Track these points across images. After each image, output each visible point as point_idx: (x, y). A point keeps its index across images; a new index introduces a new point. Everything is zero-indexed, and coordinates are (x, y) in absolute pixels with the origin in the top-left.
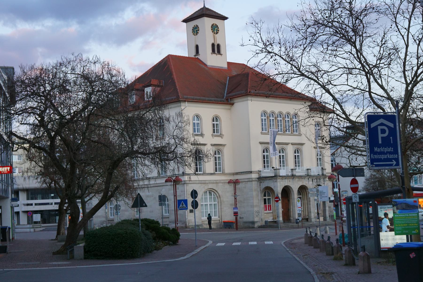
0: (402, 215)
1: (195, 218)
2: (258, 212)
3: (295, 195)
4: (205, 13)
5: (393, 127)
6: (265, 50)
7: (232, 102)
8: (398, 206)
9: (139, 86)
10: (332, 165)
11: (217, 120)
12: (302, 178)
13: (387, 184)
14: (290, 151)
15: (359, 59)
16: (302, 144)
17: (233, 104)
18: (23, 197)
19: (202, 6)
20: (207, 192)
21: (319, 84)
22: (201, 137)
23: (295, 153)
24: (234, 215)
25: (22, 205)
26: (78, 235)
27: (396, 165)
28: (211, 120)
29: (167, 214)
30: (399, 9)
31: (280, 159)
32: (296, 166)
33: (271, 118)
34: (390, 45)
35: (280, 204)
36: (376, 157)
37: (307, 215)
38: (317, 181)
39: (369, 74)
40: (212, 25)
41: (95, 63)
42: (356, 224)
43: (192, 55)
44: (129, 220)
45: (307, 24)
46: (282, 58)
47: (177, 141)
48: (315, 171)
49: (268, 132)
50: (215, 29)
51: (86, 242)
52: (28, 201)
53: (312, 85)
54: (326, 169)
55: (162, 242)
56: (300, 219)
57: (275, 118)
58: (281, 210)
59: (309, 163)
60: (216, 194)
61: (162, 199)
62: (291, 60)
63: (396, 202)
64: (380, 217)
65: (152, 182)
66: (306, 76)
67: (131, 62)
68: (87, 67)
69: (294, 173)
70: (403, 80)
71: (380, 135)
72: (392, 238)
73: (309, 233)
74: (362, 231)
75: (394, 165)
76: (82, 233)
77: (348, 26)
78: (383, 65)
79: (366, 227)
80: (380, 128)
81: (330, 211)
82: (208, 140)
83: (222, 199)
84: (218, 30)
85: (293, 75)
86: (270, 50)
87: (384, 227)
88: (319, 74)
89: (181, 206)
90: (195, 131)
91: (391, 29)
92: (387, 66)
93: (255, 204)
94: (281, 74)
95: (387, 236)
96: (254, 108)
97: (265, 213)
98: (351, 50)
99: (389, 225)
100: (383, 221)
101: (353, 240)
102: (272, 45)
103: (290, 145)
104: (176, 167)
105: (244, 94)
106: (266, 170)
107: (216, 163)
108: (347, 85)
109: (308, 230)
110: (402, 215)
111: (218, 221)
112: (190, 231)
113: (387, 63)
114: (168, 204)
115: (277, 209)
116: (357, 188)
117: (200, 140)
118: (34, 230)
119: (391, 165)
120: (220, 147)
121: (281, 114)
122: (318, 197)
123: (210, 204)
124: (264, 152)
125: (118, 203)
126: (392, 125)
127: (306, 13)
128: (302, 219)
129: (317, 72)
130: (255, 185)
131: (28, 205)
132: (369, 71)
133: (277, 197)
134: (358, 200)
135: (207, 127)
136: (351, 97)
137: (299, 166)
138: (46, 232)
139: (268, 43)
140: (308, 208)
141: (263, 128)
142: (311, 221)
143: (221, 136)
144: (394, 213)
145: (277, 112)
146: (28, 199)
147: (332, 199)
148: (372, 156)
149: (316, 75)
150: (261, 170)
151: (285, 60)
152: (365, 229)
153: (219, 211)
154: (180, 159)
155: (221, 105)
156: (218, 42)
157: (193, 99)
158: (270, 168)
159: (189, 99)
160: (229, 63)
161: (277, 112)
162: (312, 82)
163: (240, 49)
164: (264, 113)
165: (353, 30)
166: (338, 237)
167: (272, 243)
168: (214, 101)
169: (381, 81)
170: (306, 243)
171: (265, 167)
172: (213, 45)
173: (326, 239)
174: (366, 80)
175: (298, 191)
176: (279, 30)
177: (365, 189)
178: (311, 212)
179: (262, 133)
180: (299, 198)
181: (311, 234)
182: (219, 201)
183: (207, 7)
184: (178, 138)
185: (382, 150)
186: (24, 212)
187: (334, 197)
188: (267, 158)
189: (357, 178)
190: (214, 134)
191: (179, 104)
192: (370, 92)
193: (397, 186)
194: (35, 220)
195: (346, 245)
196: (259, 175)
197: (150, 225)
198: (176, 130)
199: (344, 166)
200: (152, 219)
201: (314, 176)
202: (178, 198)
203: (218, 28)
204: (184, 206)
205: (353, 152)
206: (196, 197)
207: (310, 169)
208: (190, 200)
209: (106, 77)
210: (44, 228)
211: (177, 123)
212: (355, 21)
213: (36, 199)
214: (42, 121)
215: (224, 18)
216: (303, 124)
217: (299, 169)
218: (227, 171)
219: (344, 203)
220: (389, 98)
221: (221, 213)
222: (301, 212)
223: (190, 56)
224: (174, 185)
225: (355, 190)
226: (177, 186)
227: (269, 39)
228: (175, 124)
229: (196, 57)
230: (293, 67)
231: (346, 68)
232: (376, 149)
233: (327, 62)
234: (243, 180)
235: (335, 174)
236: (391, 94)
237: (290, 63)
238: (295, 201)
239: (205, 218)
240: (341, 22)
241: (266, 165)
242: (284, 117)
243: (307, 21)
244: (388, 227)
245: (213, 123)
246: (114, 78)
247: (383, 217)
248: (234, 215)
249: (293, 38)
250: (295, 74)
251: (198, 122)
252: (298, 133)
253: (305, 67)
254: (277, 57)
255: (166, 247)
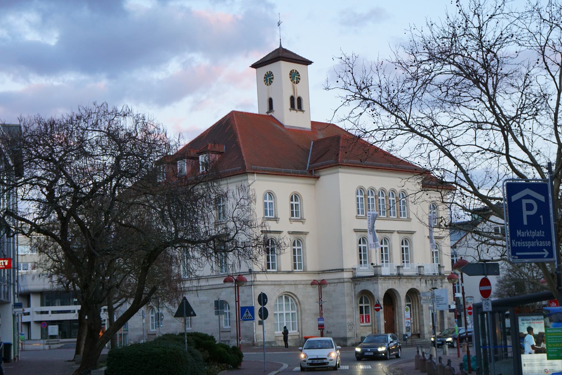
0: (557, 331)
1: (268, 331)
2: (352, 325)
3: (402, 302)
4: (281, 55)
5: (544, 201)
6: (359, 96)
7: (317, 175)
8: (552, 316)
9: (193, 154)
10: (453, 261)
11: (296, 199)
12: (412, 279)
13: (527, 288)
14: (396, 241)
15: (494, 109)
16: (412, 233)
17: (318, 178)
18: (35, 301)
19: (278, 47)
20: (282, 297)
21: (435, 144)
22: (275, 222)
23: (402, 244)
24: (319, 329)
25: (34, 313)
26: (99, 355)
27: (548, 257)
28: (288, 199)
29: (228, 327)
30: (547, 40)
31: (382, 252)
32: (404, 262)
33: (370, 197)
34: (535, 89)
35: (381, 314)
36: (520, 244)
37: (418, 329)
38: (432, 283)
39: (505, 129)
40: (291, 72)
41: (125, 115)
42: (487, 343)
43: (264, 111)
44: (172, 334)
45: (418, 59)
46: (384, 107)
47: (238, 225)
48: (430, 269)
49: (366, 215)
50: (295, 77)
51: (107, 365)
52: (42, 307)
53: (426, 145)
54: (444, 267)
55: (218, 366)
56: (409, 334)
57: (375, 196)
58: (382, 323)
59: (422, 257)
60: (295, 300)
61: (220, 306)
62: (396, 110)
63: (548, 311)
64: (522, 333)
65: (203, 283)
66: (416, 132)
67: (181, 123)
68: (114, 122)
69: (401, 271)
70: (554, 139)
71: (525, 213)
72: (539, 362)
73: (421, 354)
74: (496, 352)
75: (545, 256)
76: (105, 351)
77: (477, 61)
78: (526, 116)
79: (501, 346)
80: (524, 202)
81: (450, 324)
82: (284, 225)
83: (302, 307)
84: (300, 79)
85: (399, 131)
86: (367, 96)
87: (527, 347)
88: (435, 130)
89: (245, 315)
90: (266, 214)
91: (537, 65)
92: (531, 117)
93: (347, 314)
94: (381, 130)
95: (532, 360)
96: (347, 183)
97: (361, 326)
98: (481, 95)
99: (535, 344)
100: (527, 338)
101: (483, 365)
102: (368, 89)
103: (396, 233)
104: (237, 261)
105: (332, 165)
106: (363, 268)
107: (295, 257)
108: (476, 145)
109: (420, 350)
110: (557, 331)
111: (297, 337)
112: (257, 350)
113: (532, 113)
114: (229, 313)
115: (378, 321)
116: (490, 291)
117: (272, 226)
118: (50, 347)
119: (542, 256)
120: (301, 236)
121: (383, 191)
122: (433, 304)
123: (286, 314)
124: (360, 243)
125: (160, 311)
126: (542, 198)
127: (417, 45)
128: (412, 335)
129: (433, 127)
130: (347, 287)
131: (42, 313)
132: (505, 125)
133: (378, 305)
134: (490, 309)
135: (283, 208)
136: (480, 162)
137: (407, 262)
138: (63, 350)
139: (363, 86)
140: (419, 319)
141: (358, 210)
142: (424, 338)
143: (302, 220)
144: (546, 327)
145: (377, 188)
146: (42, 305)
147: (453, 307)
148: (513, 243)
149: (431, 130)
150: (356, 267)
151: (387, 110)
152: (499, 349)
153: (298, 323)
154: (244, 251)
155: (302, 178)
156: (299, 94)
157: (264, 171)
158: (368, 264)
159: (259, 170)
160: (313, 123)
161: (377, 188)
162: (426, 140)
163: (327, 105)
164: (361, 190)
165: (483, 66)
166: (461, 360)
167: (370, 368)
168: (293, 173)
169: (523, 140)
170: (417, 369)
171: (361, 263)
172: (292, 98)
173: (445, 363)
174: (503, 138)
175: (406, 296)
176: (379, 67)
177: (499, 294)
178: (423, 325)
179: (357, 217)
180: (407, 305)
181: (423, 355)
182: (299, 310)
183: (284, 47)
184: (239, 220)
185: (528, 234)
186: (37, 322)
187: (456, 304)
188: (364, 251)
189: (489, 277)
190: (292, 218)
191: (245, 178)
192: (508, 156)
193: (546, 289)
194: (50, 333)
195: (472, 372)
196: (354, 274)
197: (202, 341)
198: (237, 210)
199: (470, 260)
200: (204, 332)
201: (428, 276)
202: (241, 305)
203: (299, 76)
204: (250, 315)
205: (483, 240)
206: (265, 303)
207: (423, 267)
208: (258, 307)
209: (139, 136)
210: (63, 345)
211: (239, 200)
212: (486, 55)
213: (53, 305)
214: (51, 196)
215: (307, 63)
216: (412, 200)
217: (407, 266)
218: (309, 269)
219: (470, 313)
220: (534, 164)
221: (302, 325)
222: (410, 325)
223: (261, 113)
224: (235, 287)
225: (486, 294)
226: (241, 289)
227: (365, 81)
228: (235, 202)
229: (270, 114)
230: (399, 120)
231: (473, 122)
232: (519, 233)
233: (446, 114)
234: (331, 281)
235: (457, 272)
236: (537, 158)
237: (393, 114)
238: (403, 310)
239: (280, 332)
240: (466, 55)
241: (363, 260)
242: (388, 195)
243: (418, 54)
244: (533, 347)
245: (292, 203)
246: (152, 137)
247: (526, 332)
248: (319, 329)
249: (398, 78)
250: (402, 130)
251: (271, 201)
252: (406, 218)
253: (415, 120)
254: (377, 106)
255: (223, 372)
